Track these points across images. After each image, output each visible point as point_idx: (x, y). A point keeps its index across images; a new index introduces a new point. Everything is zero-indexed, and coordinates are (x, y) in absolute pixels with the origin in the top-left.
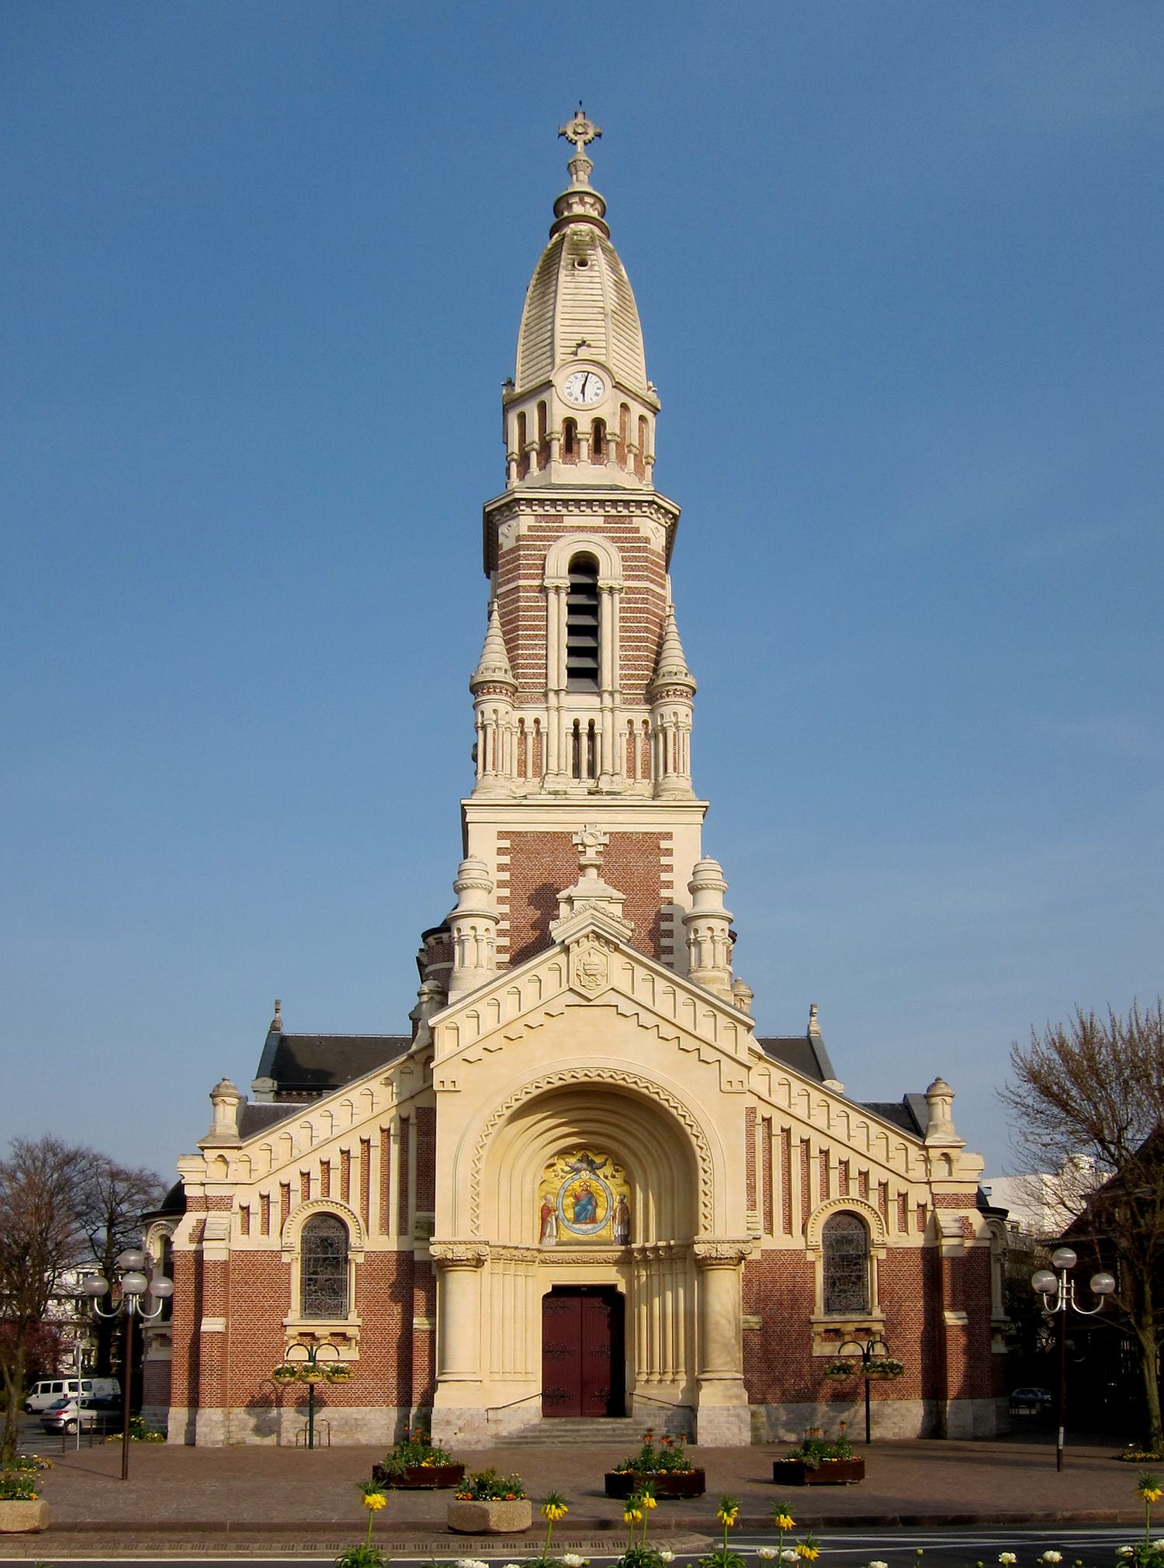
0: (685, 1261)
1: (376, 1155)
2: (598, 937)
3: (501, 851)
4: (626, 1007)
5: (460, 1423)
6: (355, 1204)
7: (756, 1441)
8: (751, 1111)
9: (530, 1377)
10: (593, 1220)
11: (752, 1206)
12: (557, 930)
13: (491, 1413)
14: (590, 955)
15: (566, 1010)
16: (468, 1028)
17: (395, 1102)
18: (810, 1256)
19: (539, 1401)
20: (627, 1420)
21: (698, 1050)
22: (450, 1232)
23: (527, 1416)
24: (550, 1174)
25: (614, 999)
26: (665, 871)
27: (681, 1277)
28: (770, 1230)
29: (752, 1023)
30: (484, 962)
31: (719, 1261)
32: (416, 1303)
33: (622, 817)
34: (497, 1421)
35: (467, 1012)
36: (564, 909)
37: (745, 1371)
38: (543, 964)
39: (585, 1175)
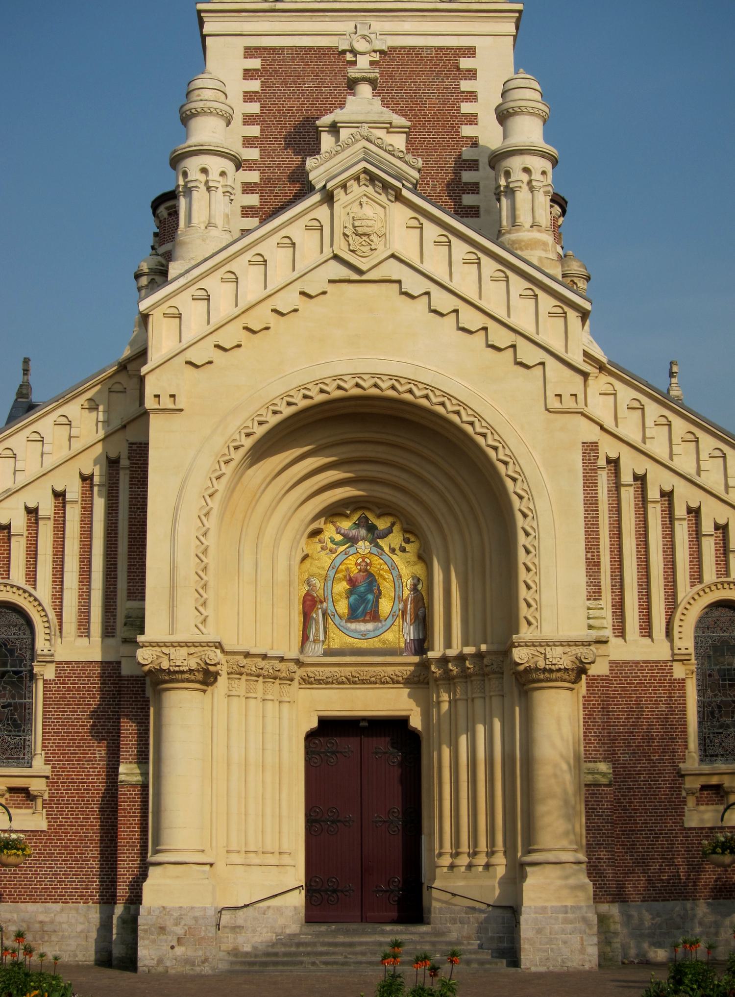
0: (502, 678)
1: (73, 515)
2: (373, 179)
3: (248, 74)
4: (414, 284)
5: (179, 931)
6: (44, 590)
7: (604, 960)
8: (591, 448)
9: (286, 859)
10: (375, 616)
11: (595, 593)
12: (318, 170)
13: (226, 918)
14: (360, 205)
15: (330, 288)
16: (195, 319)
17: (101, 434)
18: (679, 672)
19: (298, 899)
20: (424, 928)
21: (511, 346)
22: (168, 626)
23: (281, 921)
24: (315, 547)
25: (393, 270)
26: (467, 100)
27: (496, 702)
28: (621, 631)
29: (587, 306)
30: (219, 221)
31: (547, 675)
32: (123, 741)
33: (408, 26)
34: (236, 929)
35: (192, 290)
36: (327, 141)
37: (590, 849)
38: (300, 223)
39: (364, 547)
